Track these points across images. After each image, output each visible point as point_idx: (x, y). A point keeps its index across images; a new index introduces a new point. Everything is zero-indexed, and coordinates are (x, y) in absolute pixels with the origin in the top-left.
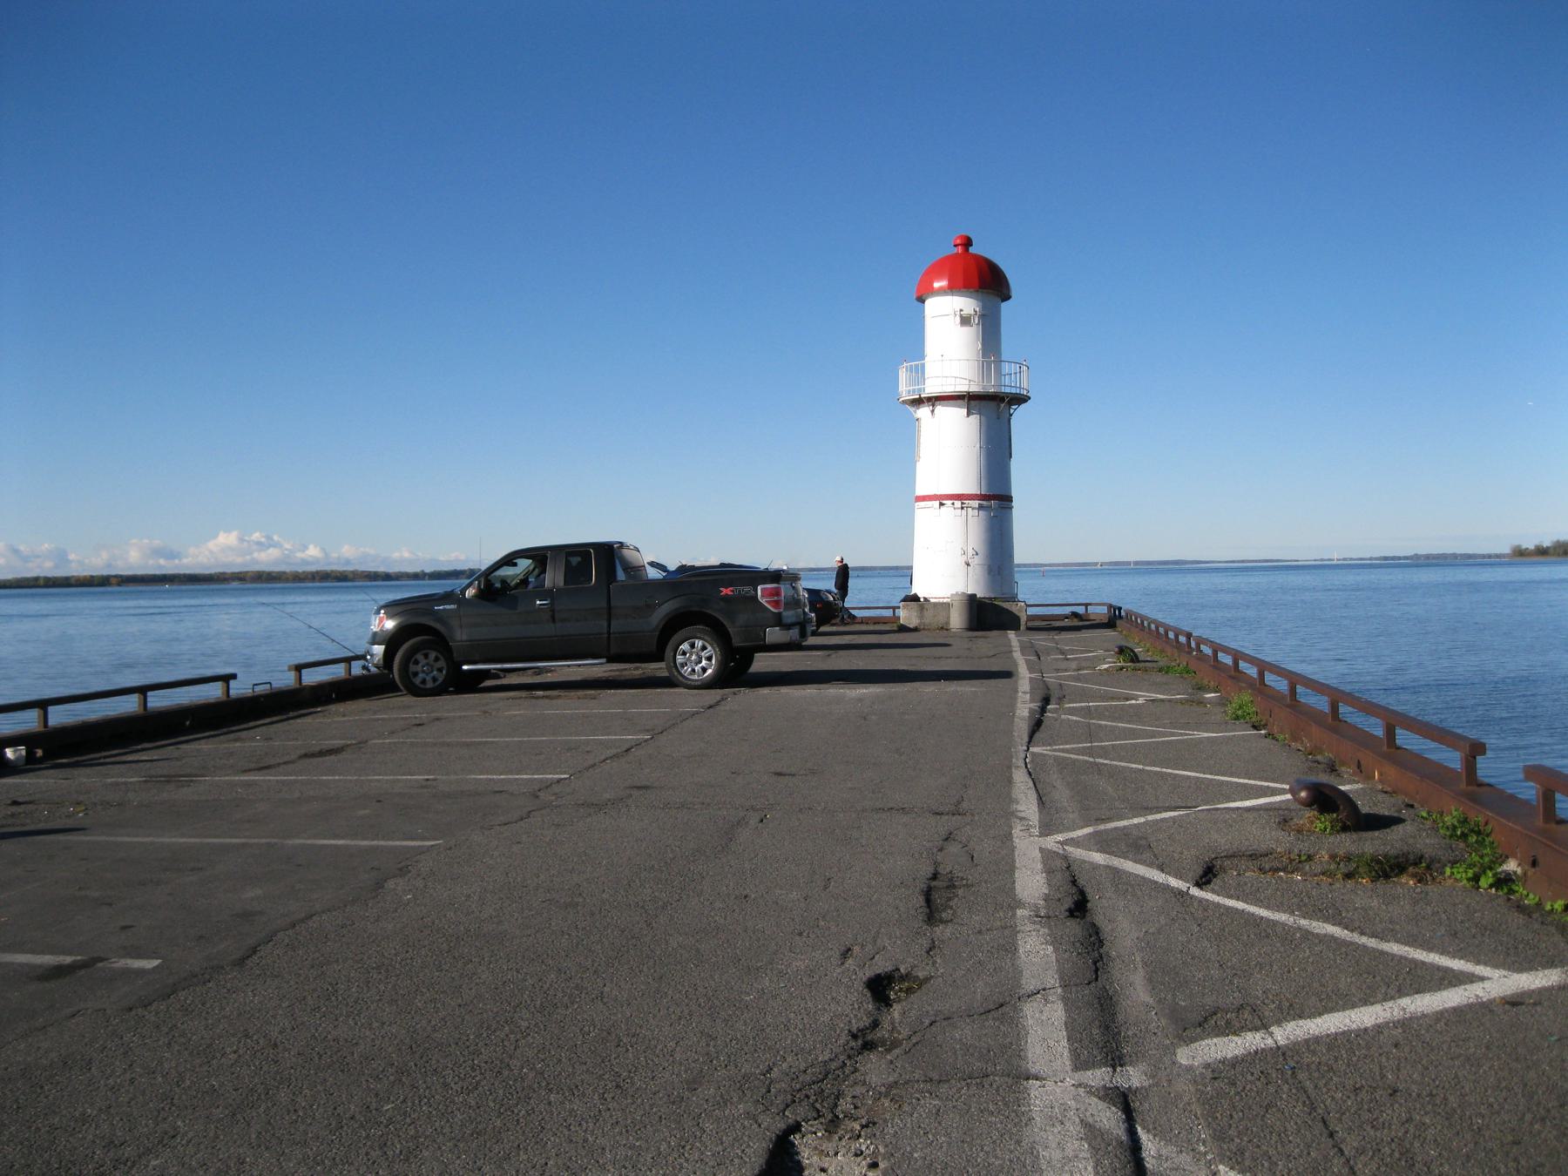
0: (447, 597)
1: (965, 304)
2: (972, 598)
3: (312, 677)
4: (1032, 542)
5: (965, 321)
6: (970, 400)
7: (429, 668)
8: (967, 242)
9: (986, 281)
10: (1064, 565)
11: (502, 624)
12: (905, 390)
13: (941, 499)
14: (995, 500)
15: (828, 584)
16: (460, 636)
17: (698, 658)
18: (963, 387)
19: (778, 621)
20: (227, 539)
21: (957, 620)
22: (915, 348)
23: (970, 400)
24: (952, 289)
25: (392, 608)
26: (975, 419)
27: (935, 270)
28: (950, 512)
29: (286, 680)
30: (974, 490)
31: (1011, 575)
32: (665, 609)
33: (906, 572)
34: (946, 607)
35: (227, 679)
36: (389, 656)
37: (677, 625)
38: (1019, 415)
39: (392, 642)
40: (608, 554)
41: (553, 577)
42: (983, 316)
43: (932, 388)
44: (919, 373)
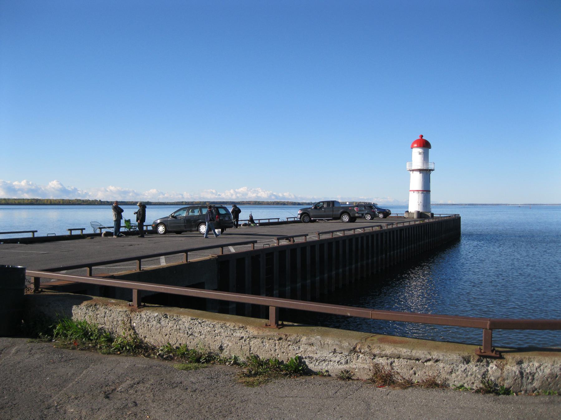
0: (310, 208)
1: (420, 150)
2: (418, 212)
3: (289, 220)
4: (434, 198)
5: (420, 153)
6: (420, 171)
7: (306, 219)
8: (422, 136)
9: (425, 145)
10: (552, 205)
11: (317, 213)
12: (408, 168)
13: (414, 191)
14: (426, 191)
15: (60, 186)
16: (311, 214)
17: (346, 218)
18: (420, 168)
19: (357, 213)
20: (154, 191)
21: (415, 216)
22: (410, 160)
23: (420, 171)
24: (417, 147)
25: (301, 210)
26: (421, 174)
27: (414, 143)
28: (416, 193)
29: (286, 220)
30: (421, 189)
31: (430, 206)
32: (341, 211)
33: (407, 207)
34: (413, 213)
35: (278, 219)
36: (301, 217)
37: (343, 213)
38: (432, 173)
39: (301, 215)
40: (333, 202)
41: (325, 206)
42: (424, 153)
43: (413, 168)
44: (411, 165)
